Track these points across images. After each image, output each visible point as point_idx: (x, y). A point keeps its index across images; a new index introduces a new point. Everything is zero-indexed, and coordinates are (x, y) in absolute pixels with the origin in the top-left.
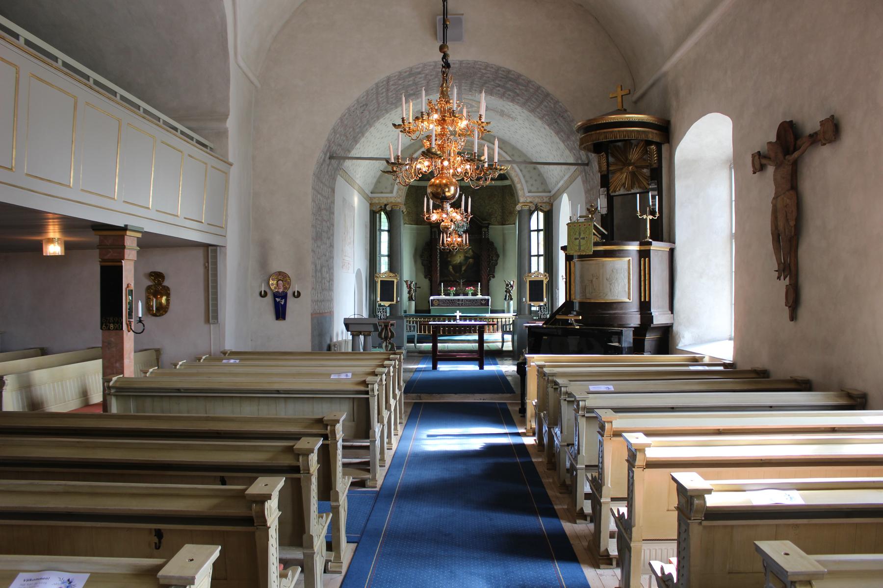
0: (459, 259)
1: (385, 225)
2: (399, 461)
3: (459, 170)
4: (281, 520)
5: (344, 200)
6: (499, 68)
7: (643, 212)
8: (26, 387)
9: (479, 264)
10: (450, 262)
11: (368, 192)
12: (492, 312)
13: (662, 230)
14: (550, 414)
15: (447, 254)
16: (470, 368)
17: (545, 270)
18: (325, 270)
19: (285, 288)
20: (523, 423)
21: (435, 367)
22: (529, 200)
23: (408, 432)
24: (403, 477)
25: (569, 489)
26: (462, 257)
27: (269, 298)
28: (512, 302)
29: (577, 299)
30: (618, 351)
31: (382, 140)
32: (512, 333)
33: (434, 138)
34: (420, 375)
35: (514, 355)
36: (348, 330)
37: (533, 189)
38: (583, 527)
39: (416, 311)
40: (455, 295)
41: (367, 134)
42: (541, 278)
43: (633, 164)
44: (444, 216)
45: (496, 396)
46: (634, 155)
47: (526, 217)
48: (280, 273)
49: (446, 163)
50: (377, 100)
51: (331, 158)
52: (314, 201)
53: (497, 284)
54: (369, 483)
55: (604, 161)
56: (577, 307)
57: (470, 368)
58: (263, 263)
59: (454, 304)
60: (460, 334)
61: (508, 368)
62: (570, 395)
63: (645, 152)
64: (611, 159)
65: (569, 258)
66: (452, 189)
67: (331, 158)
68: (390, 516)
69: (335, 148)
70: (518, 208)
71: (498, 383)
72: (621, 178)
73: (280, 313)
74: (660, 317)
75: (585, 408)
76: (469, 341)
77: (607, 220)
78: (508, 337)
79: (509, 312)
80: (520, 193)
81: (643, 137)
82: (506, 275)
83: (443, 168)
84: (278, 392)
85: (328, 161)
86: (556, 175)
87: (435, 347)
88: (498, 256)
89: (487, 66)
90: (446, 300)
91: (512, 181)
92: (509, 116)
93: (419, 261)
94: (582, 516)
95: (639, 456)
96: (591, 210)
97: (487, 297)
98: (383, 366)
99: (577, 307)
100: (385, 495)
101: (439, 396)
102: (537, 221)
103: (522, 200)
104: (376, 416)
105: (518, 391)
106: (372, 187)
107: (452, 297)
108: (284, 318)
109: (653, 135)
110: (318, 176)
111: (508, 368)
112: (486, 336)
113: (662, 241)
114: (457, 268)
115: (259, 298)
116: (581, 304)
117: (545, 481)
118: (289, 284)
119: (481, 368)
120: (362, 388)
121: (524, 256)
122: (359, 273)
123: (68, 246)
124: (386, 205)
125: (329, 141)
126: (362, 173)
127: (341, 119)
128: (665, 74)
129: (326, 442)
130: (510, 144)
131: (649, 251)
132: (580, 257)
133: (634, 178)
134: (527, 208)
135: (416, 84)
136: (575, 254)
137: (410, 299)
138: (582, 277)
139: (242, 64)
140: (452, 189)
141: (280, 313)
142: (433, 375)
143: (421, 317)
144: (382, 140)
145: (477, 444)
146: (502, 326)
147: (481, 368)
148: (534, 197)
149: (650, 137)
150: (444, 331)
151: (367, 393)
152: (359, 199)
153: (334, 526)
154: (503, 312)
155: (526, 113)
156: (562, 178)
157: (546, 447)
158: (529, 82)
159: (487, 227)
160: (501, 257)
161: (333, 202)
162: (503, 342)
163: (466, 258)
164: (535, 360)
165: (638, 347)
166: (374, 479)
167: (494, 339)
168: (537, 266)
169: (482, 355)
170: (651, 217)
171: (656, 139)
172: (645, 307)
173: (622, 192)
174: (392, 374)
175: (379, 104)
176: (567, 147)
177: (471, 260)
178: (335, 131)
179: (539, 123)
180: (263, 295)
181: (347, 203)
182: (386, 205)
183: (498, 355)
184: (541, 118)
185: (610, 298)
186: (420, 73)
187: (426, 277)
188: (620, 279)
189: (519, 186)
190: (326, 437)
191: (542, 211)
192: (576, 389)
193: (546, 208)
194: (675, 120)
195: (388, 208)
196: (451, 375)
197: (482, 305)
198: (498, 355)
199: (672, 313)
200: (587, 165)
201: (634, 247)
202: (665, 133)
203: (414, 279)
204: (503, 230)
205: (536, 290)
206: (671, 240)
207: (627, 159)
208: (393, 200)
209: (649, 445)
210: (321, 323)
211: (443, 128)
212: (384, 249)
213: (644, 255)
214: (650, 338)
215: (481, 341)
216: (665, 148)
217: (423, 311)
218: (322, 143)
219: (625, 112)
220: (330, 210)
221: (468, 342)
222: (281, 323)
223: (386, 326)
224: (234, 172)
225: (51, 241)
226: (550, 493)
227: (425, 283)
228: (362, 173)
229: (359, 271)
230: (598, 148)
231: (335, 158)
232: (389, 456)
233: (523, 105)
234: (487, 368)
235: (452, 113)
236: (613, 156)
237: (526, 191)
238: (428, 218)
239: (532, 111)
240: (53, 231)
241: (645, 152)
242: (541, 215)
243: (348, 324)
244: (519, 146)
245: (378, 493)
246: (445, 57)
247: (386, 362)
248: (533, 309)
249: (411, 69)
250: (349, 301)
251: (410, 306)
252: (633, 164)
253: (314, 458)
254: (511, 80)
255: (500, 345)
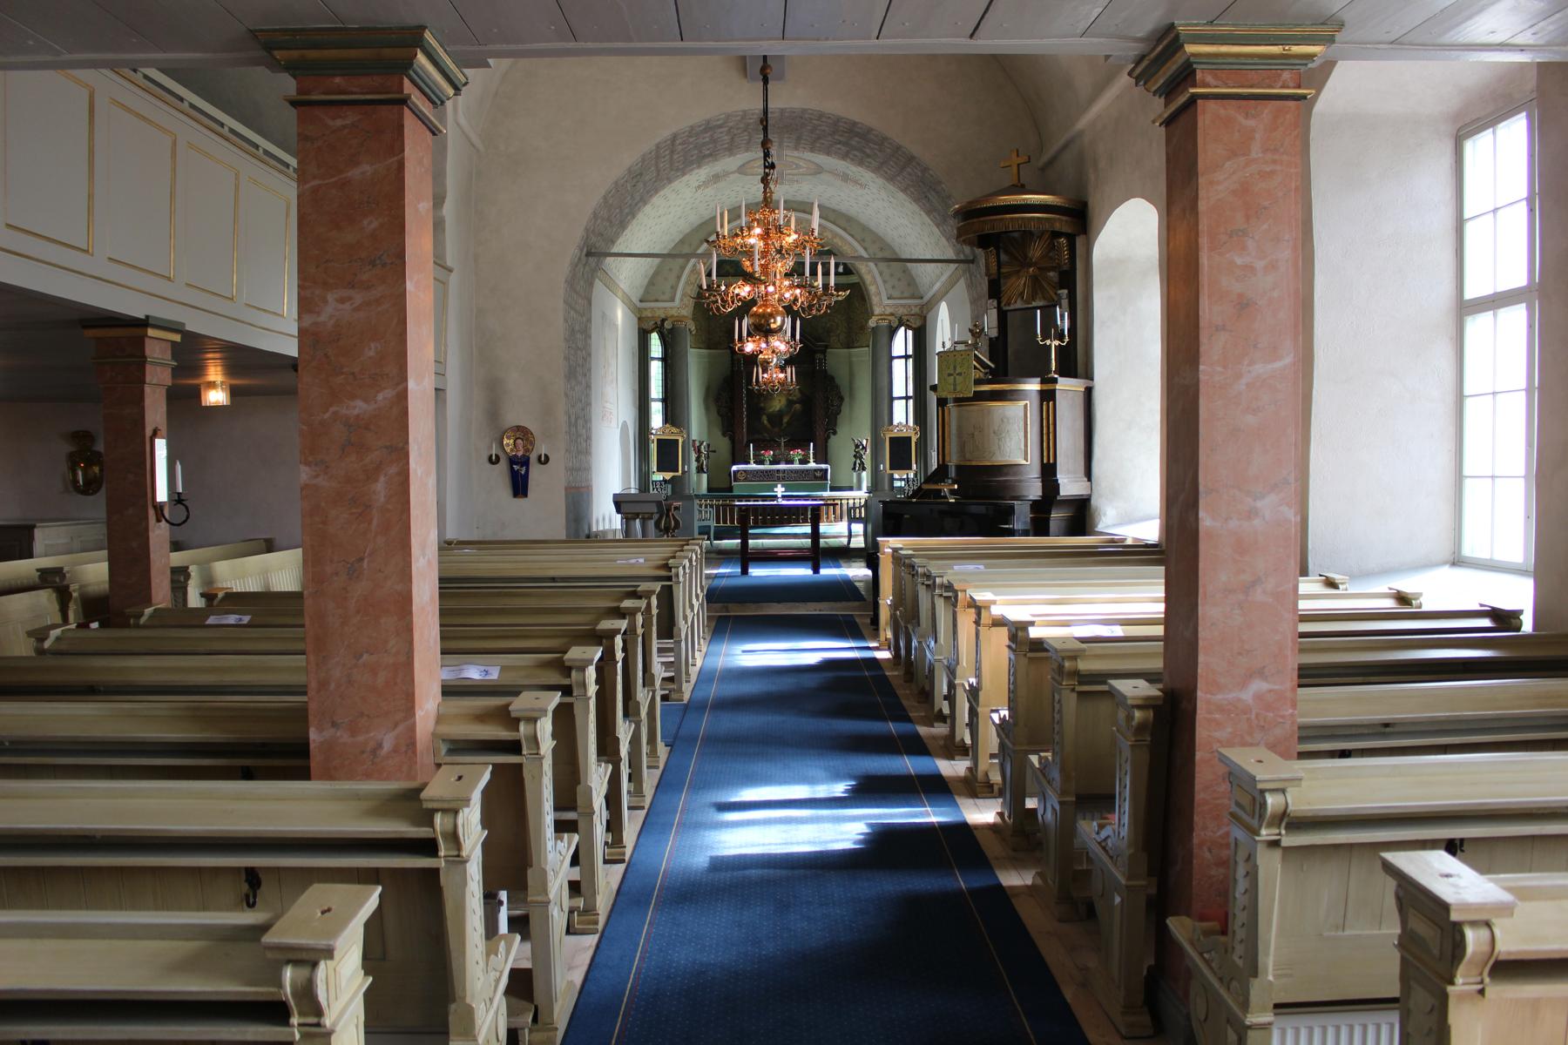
0: (777, 404)
1: (656, 348)
2: (706, 677)
3: (787, 295)
4: (487, 846)
5: (604, 315)
6: (838, 120)
7: (1046, 336)
8: (208, 580)
9: (813, 413)
10: (763, 409)
11: (635, 299)
12: (833, 489)
13: (1076, 361)
14: (908, 617)
15: (759, 398)
16: (802, 572)
17: (916, 422)
18: (580, 422)
19: (527, 450)
20: (875, 633)
21: (745, 572)
22: (889, 311)
23: (715, 648)
24: (713, 691)
25: (926, 695)
26: (784, 401)
27: (503, 465)
28: (864, 474)
29: (953, 461)
30: (1011, 533)
31: (660, 222)
32: (864, 521)
33: (757, 257)
34: (724, 582)
35: (870, 556)
36: (618, 511)
37: (896, 294)
38: (941, 729)
39: (709, 490)
40: (772, 463)
41: (640, 216)
42: (911, 433)
43: (1035, 264)
44: (763, 345)
45: (839, 605)
46: (1036, 251)
47: (885, 339)
48: (519, 428)
49: (771, 289)
50: (657, 165)
51: (589, 254)
52: (566, 321)
53: (841, 445)
54: (674, 696)
55: (993, 259)
56: (952, 473)
57: (802, 572)
58: (493, 413)
59: (773, 477)
60: (782, 524)
61: (857, 572)
62: (928, 576)
63: (1052, 247)
64: (1003, 257)
65: (942, 403)
66: (779, 319)
67: (589, 254)
68: (705, 724)
69: (594, 239)
70: (872, 323)
71: (844, 590)
72: (1018, 284)
73: (520, 487)
74: (1070, 485)
75: (942, 586)
76: (795, 536)
77: (998, 348)
78: (858, 528)
79: (859, 488)
80: (875, 300)
81: (1047, 226)
82: (855, 430)
83: (767, 294)
84: (553, 579)
85: (584, 259)
86: (931, 277)
87: (745, 544)
88: (841, 399)
89: (821, 115)
90: (757, 471)
91: (861, 277)
92: (856, 182)
93: (714, 409)
94: (941, 718)
95: (984, 613)
96: (976, 332)
97: (823, 466)
98: (619, 613)
99: (952, 473)
100: (696, 707)
101: (753, 606)
102: (902, 342)
103: (877, 310)
104: (640, 674)
105: (870, 598)
106: (641, 291)
107: (767, 467)
108: (525, 495)
109: (1062, 224)
110: (571, 283)
111: (857, 572)
112: (823, 528)
113: (1075, 376)
114: (776, 418)
115: (489, 465)
116: (958, 468)
117: (900, 692)
118: (532, 444)
119: (816, 571)
120: (663, 573)
121: (882, 399)
122: (624, 427)
123: (234, 392)
124: (663, 321)
125: (587, 230)
126: (627, 274)
127: (605, 198)
128: (1081, 134)
129: (567, 700)
130: (858, 223)
131: (1053, 392)
132: (957, 400)
133: (1036, 286)
134: (885, 323)
135: (714, 141)
136: (950, 396)
137: (700, 470)
138: (960, 428)
139: (463, 121)
140: (779, 319)
141: (520, 487)
142: (743, 581)
143: (718, 498)
144: (660, 222)
145: (812, 659)
146: (849, 510)
147: (816, 571)
148: (897, 306)
149: (1057, 227)
150: (756, 521)
151: (428, 847)
152: (624, 314)
153: (614, 781)
154: (851, 489)
155: (880, 181)
156: (938, 277)
157: (907, 663)
158: (885, 139)
159: (824, 353)
160: (847, 400)
161: (589, 320)
162: (850, 536)
163: (790, 403)
164: (890, 544)
165: (1040, 526)
166: (680, 690)
167: (835, 531)
168: (902, 414)
169: (817, 554)
170: (1057, 343)
171: (1066, 229)
172: (1048, 472)
173: (1019, 305)
174: (640, 631)
175: (658, 171)
176: (944, 233)
177: (798, 406)
178: (595, 215)
179: (901, 195)
180: (494, 461)
181: (607, 319)
182: (663, 321)
183: (843, 554)
184: (904, 190)
185: (999, 460)
186: (720, 126)
187: (724, 435)
188: (1013, 435)
189: (872, 289)
190: (567, 691)
191: (908, 327)
192: (934, 568)
193: (918, 324)
194: (1094, 202)
195: (667, 325)
196: (770, 581)
197: (816, 478)
198: (843, 554)
199: (1089, 479)
200: (972, 262)
201: (1033, 386)
202: (1080, 220)
203: (705, 438)
204: (850, 355)
205: (900, 452)
206: (1089, 376)
207: (1026, 257)
208: (674, 312)
209: (994, 602)
210: (578, 501)
211: (766, 244)
212: (656, 389)
213: (1047, 396)
214: (1057, 516)
215: (815, 535)
216: (1079, 241)
217: (721, 488)
218: (579, 233)
219: (1021, 188)
220: (586, 332)
221: (796, 534)
222: (520, 501)
223: (668, 510)
224: (453, 279)
225: (212, 385)
226: (905, 703)
227: (723, 444)
228: (627, 274)
229: (625, 425)
230: (984, 241)
231: (594, 254)
232: (694, 671)
233: (876, 170)
234: (824, 572)
235: (779, 229)
236: (1006, 252)
237: (884, 297)
238: (741, 349)
239: (891, 179)
240: (215, 373)
241: (1052, 247)
242: (910, 333)
243: (619, 502)
244: (872, 225)
245: (686, 707)
246: (767, 155)
247: (628, 603)
248: (897, 484)
249: (708, 122)
250: (612, 472)
251: (699, 481)
252: (1035, 264)
253: (545, 727)
254: (857, 135)
255: (845, 541)
